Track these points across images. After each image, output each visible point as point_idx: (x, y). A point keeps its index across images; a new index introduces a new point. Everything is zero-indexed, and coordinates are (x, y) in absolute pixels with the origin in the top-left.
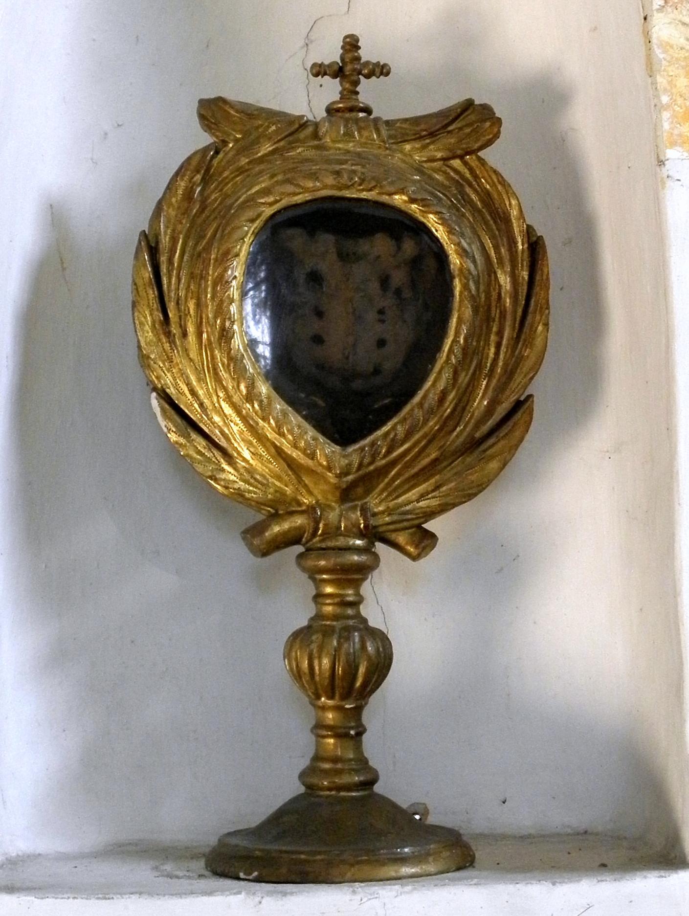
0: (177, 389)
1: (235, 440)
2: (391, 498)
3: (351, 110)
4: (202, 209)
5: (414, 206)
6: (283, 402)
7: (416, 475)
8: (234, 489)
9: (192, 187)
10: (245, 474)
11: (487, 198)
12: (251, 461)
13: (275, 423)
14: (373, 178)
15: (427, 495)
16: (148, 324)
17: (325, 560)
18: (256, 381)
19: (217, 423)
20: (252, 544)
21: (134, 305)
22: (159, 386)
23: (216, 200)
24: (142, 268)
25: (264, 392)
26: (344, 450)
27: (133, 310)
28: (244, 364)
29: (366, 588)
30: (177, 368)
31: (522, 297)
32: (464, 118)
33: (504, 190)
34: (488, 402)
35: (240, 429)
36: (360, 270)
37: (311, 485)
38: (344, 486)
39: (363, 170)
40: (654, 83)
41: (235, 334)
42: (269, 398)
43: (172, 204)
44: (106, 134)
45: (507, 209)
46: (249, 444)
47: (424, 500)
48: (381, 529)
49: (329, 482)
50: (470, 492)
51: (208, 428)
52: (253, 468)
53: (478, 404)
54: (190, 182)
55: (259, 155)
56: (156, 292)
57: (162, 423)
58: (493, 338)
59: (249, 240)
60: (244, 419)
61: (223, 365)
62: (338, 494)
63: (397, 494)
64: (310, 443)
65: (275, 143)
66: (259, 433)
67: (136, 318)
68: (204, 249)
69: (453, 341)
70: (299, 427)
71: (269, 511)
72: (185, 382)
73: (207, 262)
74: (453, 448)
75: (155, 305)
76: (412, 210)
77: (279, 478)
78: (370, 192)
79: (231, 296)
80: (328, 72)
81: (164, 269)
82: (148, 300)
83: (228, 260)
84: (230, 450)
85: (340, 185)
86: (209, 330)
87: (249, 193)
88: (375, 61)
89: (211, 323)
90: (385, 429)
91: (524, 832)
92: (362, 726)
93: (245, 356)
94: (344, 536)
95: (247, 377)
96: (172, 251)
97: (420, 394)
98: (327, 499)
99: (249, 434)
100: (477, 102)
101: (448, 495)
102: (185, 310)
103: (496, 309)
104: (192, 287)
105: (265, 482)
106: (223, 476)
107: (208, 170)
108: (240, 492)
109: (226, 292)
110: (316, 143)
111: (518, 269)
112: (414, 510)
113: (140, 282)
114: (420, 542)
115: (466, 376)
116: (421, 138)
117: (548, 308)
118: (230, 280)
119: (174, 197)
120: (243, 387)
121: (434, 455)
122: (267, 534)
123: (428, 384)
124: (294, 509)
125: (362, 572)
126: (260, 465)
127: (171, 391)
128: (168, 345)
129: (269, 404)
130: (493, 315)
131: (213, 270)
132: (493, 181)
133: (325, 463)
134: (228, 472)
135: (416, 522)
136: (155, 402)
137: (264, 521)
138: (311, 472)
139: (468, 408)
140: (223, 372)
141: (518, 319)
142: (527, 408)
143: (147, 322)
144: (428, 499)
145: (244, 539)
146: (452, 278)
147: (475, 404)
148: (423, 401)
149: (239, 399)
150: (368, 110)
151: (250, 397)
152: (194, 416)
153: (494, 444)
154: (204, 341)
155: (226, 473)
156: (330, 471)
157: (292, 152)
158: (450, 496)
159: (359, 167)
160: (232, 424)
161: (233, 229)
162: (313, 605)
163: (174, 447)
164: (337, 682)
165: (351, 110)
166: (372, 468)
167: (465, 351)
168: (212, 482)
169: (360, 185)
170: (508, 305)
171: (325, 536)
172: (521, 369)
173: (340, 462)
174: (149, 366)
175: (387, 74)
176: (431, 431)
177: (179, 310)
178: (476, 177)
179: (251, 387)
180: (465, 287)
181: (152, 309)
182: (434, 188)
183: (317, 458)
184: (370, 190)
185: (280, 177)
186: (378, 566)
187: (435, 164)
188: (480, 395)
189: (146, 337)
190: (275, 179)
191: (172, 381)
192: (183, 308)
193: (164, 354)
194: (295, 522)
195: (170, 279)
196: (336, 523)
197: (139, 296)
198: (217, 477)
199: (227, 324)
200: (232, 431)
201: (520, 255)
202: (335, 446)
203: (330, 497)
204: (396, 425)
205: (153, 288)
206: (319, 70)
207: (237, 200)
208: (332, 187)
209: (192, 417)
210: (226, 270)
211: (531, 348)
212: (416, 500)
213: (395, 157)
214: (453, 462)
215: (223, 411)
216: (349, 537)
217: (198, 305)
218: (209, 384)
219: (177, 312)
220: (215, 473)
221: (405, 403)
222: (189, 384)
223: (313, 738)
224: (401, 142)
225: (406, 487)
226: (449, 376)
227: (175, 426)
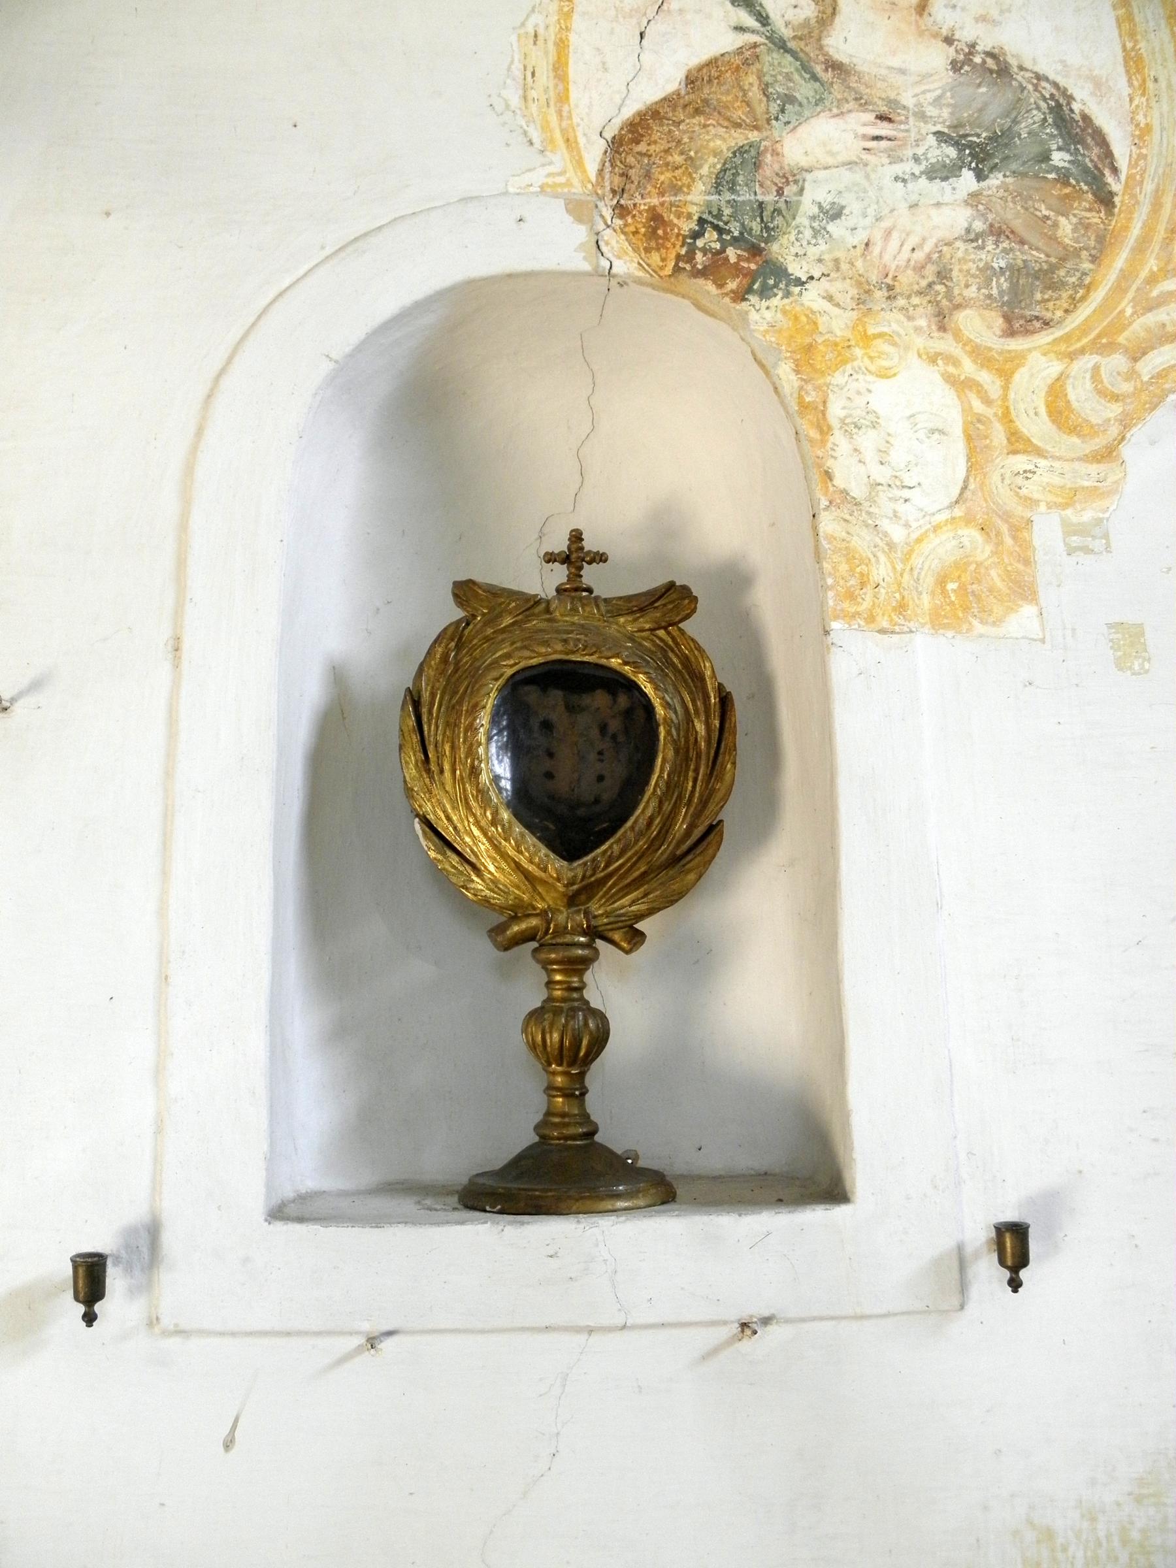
3: (576, 589)
4: (456, 670)
5: (627, 668)
7: (629, 885)
8: (482, 896)
11: (686, 661)
12: (495, 874)
14: (594, 645)
21: (401, 747)
22: (421, 813)
27: (400, 751)
29: (588, 977)
36: (583, 720)
37: (544, 893)
38: (571, 894)
39: (586, 639)
40: (821, 568)
42: (509, 822)
44: (378, 609)
46: (494, 860)
48: (600, 929)
49: (559, 891)
50: (672, 898)
57: (424, 843)
58: (691, 774)
61: (473, 796)
65: (514, 617)
69: (658, 777)
70: (534, 846)
73: (460, 712)
77: (518, 887)
81: (425, 718)
84: (478, 865)
90: (604, 848)
92: (585, 1087)
94: (571, 934)
96: (432, 704)
98: (557, 904)
100: (677, 584)
105: (506, 890)
106: (472, 886)
110: (548, 616)
112: (627, 913)
113: (405, 729)
114: (633, 938)
117: (735, 750)
120: (488, 814)
122: (508, 933)
123: (638, 811)
127: (431, 817)
129: (510, 827)
133: (555, 875)
135: (629, 923)
136: (417, 826)
138: (544, 882)
141: (711, 759)
145: (490, 936)
146: (658, 725)
150: (589, 590)
151: (494, 822)
153: (691, 860)
160: (480, 844)
162: (545, 990)
163: (433, 863)
164: (565, 1052)
165: (576, 589)
166: (593, 879)
168: (464, 891)
169: (584, 650)
170: (703, 747)
174: (413, 797)
175: (605, 561)
177: (437, 751)
178: (677, 644)
179: (495, 813)
180: (669, 733)
185: (518, 644)
187: (644, 634)
190: (515, 646)
203: (559, 902)
204: (612, 844)
206: (550, 558)
207: (484, 663)
208: (561, 652)
209: (443, 833)
210: (475, 719)
214: (658, 874)
216: (575, 935)
217: (453, 748)
221: (620, 827)
222: (445, 812)
223: (545, 1097)
225: (621, 894)
227: (435, 846)
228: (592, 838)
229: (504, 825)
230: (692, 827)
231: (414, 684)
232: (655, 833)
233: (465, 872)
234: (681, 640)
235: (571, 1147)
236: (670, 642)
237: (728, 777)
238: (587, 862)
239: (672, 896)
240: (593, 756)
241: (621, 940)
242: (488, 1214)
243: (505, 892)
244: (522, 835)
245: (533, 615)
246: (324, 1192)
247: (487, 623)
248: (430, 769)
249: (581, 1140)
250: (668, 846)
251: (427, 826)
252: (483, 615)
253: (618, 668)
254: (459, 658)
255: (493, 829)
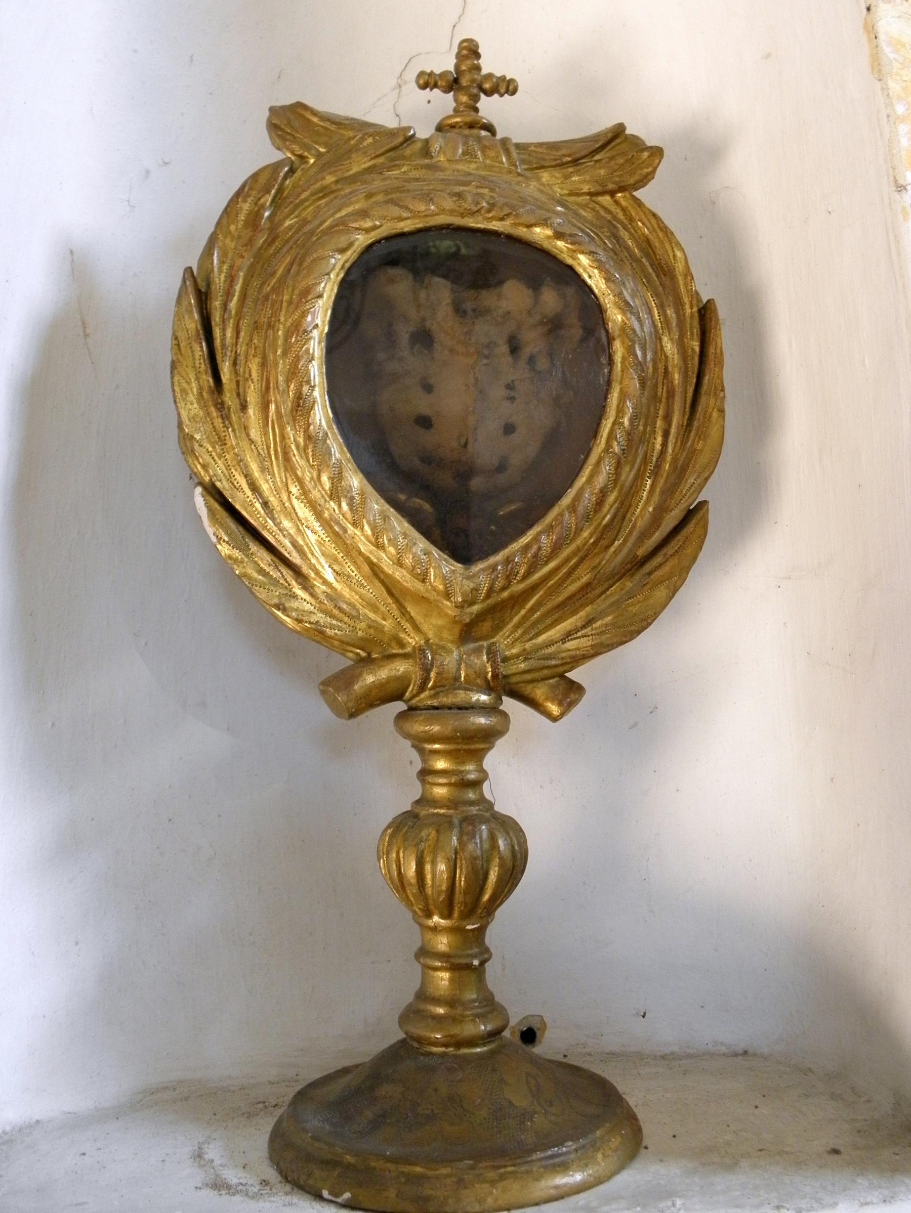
0: (231, 482)
1: (313, 554)
2: (528, 637)
3: (471, 126)
4: (270, 242)
5: (560, 244)
6: (382, 501)
7: (560, 606)
8: (310, 623)
9: (259, 210)
10: (326, 602)
11: (647, 246)
12: (335, 584)
13: (372, 530)
14: (506, 204)
15: (576, 633)
16: (193, 393)
17: (439, 725)
18: (344, 470)
19: (287, 531)
20: (335, 699)
21: (174, 366)
22: (207, 479)
23: (290, 228)
24: (187, 317)
25: (355, 486)
26: (467, 569)
27: (172, 373)
28: (328, 446)
29: (491, 761)
30: (232, 453)
31: (693, 373)
32: (613, 147)
33: (666, 239)
34: (654, 508)
35: (320, 539)
36: (484, 330)
37: (419, 619)
38: (468, 620)
39: (492, 194)
40: (885, 89)
41: (316, 404)
42: (362, 493)
43: (230, 232)
44: (148, 172)
45: (671, 262)
46: (333, 561)
47: (572, 640)
48: (514, 680)
49: (446, 614)
50: (633, 628)
51: (274, 536)
52: (337, 594)
53: (641, 510)
54: (256, 204)
55: (351, 173)
56: (205, 348)
57: (210, 530)
58: (659, 423)
59: (337, 276)
60: (327, 524)
61: (298, 447)
62: (457, 630)
63: (536, 631)
64: (420, 559)
65: (372, 159)
66: (347, 545)
67: (176, 383)
68: (273, 289)
69: (614, 424)
70: (405, 536)
71: (358, 654)
72: (243, 473)
73: (277, 306)
74: (608, 569)
75: (203, 366)
76: (557, 249)
77: (374, 608)
78: (503, 223)
79: (311, 351)
80: (439, 83)
81: (216, 318)
82: (194, 359)
83: (307, 302)
84: (305, 569)
85: (462, 211)
86: (278, 398)
87: (338, 215)
88: (498, 74)
89: (281, 389)
90: (524, 540)
91: (667, 1050)
92: (487, 950)
93: (329, 435)
94: (466, 689)
95: (331, 464)
96: (228, 294)
97: (571, 493)
98: (441, 639)
99: (333, 546)
100: (628, 132)
101: (603, 633)
102: (244, 372)
103: (663, 385)
104: (255, 341)
105: (354, 613)
106: (294, 604)
107: (280, 191)
108: (319, 627)
109: (304, 344)
110: (427, 161)
111: (687, 338)
112: (559, 652)
113: (182, 335)
114: (566, 695)
115: (630, 471)
116: (562, 165)
117: (723, 390)
118: (309, 329)
119: (234, 223)
120: (325, 478)
121: (585, 578)
122: (356, 687)
123: (582, 480)
124: (394, 651)
125: (489, 737)
126: (348, 590)
127: (222, 485)
128: (220, 420)
129: (363, 502)
130: (659, 394)
131: (285, 316)
132: (652, 226)
133: (441, 587)
134: (302, 599)
135: (561, 669)
136: (199, 499)
137: (349, 668)
138: (422, 600)
139: (629, 515)
140: (297, 457)
141: (689, 402)
142: (701, 518)
143: (191, 389)
144: (577, 638)
145: (323, 693)
146: (610, 340)
147: (638, 510)
148: (576, 503)
149: (320, 496)
150: (490, 128)
151: (335, 494)
152: (255, 521)
153: (661, 565)
154: (270, 414)
155: (300, 600)
156: (448, 599)
157: (395, 170)
158: (607, 634)
159: (487, 190)
160: (308, 532)
161: (314, 260)
162: (418, 784)
163: (225, 563)
164: (458, 897)
165: (471, 126)
166: (505, 594)
167: (630, 437)
168: (279, 613)
169: (489, 211)
170: (677, 382)
171: (438, 689)
172: (694, 467)
173: (462, 586)
174: (193, 451)
175: (514, 92)
176: (584, 545)
177: (236, 373)
178: (631, 220)
179: (337, 477)
180: (631, 351)
181: (199, 372)
182: (584, 225)
183: (430, 579)
184: (502, 219)
185: (380, 198)
186: (508, 730)
187: (580, 199)
188: (644, 498)
189: (190, 410)
190: (374, 199)
191: (225, 471)
192: (242, 370)
193: (214, 433)
194: (396, 669)
195: (224, 330)
196: (454, 670)
197: (181, 354)
198: (287, 605)
199: (305, 389)
200: (308, 541)
201: (688, 320)
202: (456, 564)
203: (446, 634)
204: (539, 534)
205: (201, 343)
206: (427, 82)
207: (321, 224)
208: (452, 212)
209: (252, 521)
210: (304, 315)
211: (705, 440)
212: (562, 640)
213: (530, 185)
214: (608, 589)
215: (296, 514)
216: (471, 690)
217: (263, 365)
218: (277, 475)
219: (233, 377)
220: (283, 600)
221: (551, 506)
222: (247, 476)
223: (418, 968)
224: (537, 168)
225: (548, 621)
226: (610, 470)
227: (229, 535)
228: (493, 527)
229: (352, 498)
230: (661, 511)
231: (200, 267)
232: (609, 516)
233: (282, 581)
234: (637, 214)
235: (467, 1059)
236: (621, 216)
237: (714, 432)
238: (496, 565)
239: (631, 625)
240: (498, 392)
241: (547, 699)
242: (324, 1204)
243: (350, 616)
244: (385, 518)
245: (404, 158)
246: (38, 1121)
247: (325, 166)
248: (223, 403)
249: (484, 1045)
250: (625, 541)
251: (216, 500)
252: (319, 155)
253: (546, 245)
254: (277, 219)
255: (332, 503)
